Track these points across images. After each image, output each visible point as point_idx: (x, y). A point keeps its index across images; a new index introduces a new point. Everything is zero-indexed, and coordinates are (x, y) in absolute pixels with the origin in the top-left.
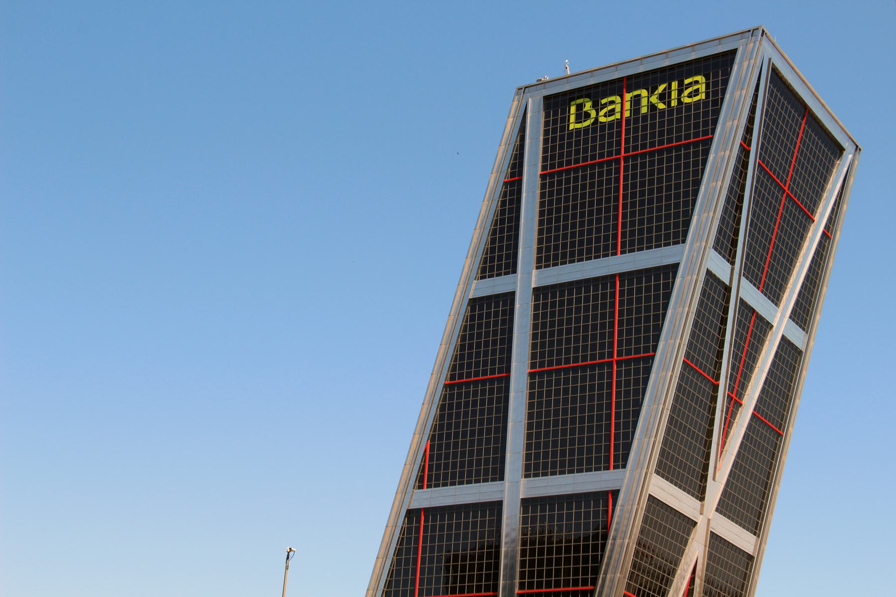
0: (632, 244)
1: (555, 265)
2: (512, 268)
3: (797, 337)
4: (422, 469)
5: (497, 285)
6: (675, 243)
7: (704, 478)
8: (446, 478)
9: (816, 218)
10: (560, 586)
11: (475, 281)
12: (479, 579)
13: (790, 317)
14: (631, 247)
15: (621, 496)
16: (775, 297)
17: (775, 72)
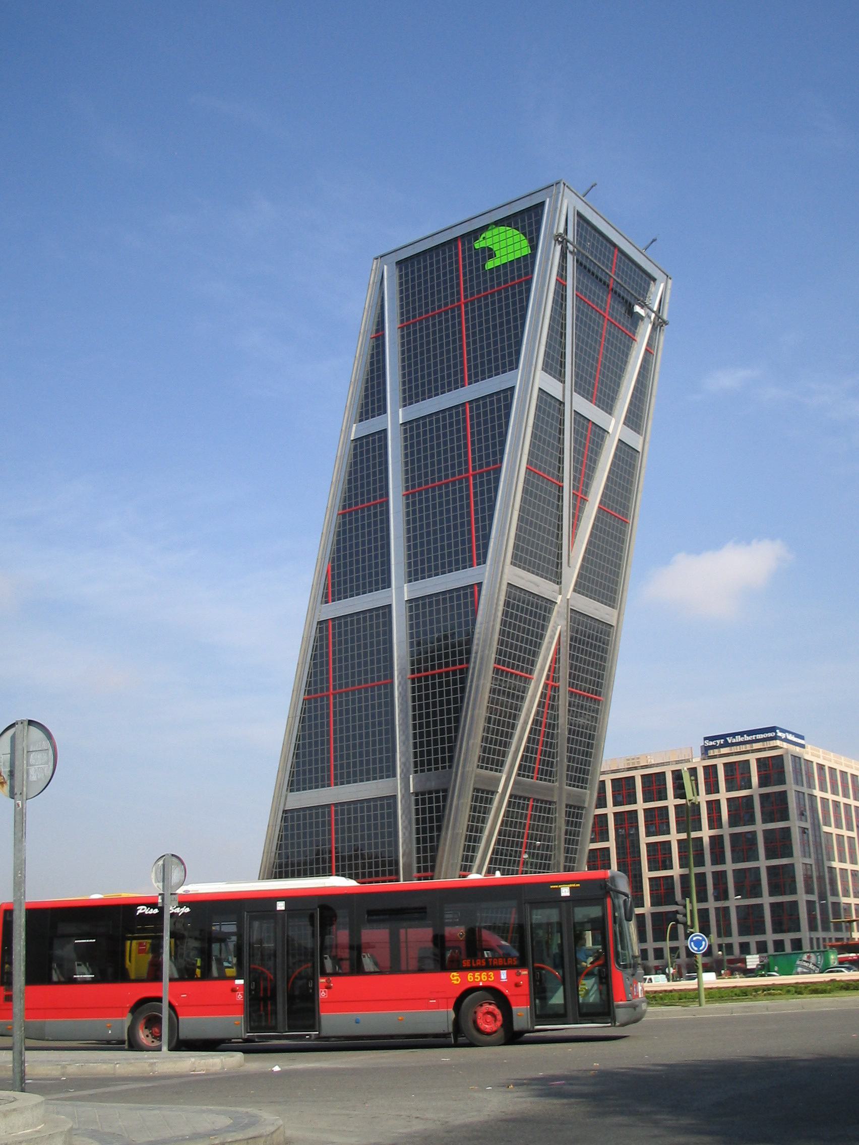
0: (476, 375)
1: (417, 401)
2: (382, 410)
3: (634, 440)
4: (326, 587)
5: (372, 426)
6: (511, 370)
7: (559, 565)
8: (345, 592)
9: (638, 338)
10: (449, 667)
11: (355, 425)
12: (379, 671)
13: (624, 423)
14: (476, 377)
15: (484, 587)
16: (608, 406)
17: (579, 215)
